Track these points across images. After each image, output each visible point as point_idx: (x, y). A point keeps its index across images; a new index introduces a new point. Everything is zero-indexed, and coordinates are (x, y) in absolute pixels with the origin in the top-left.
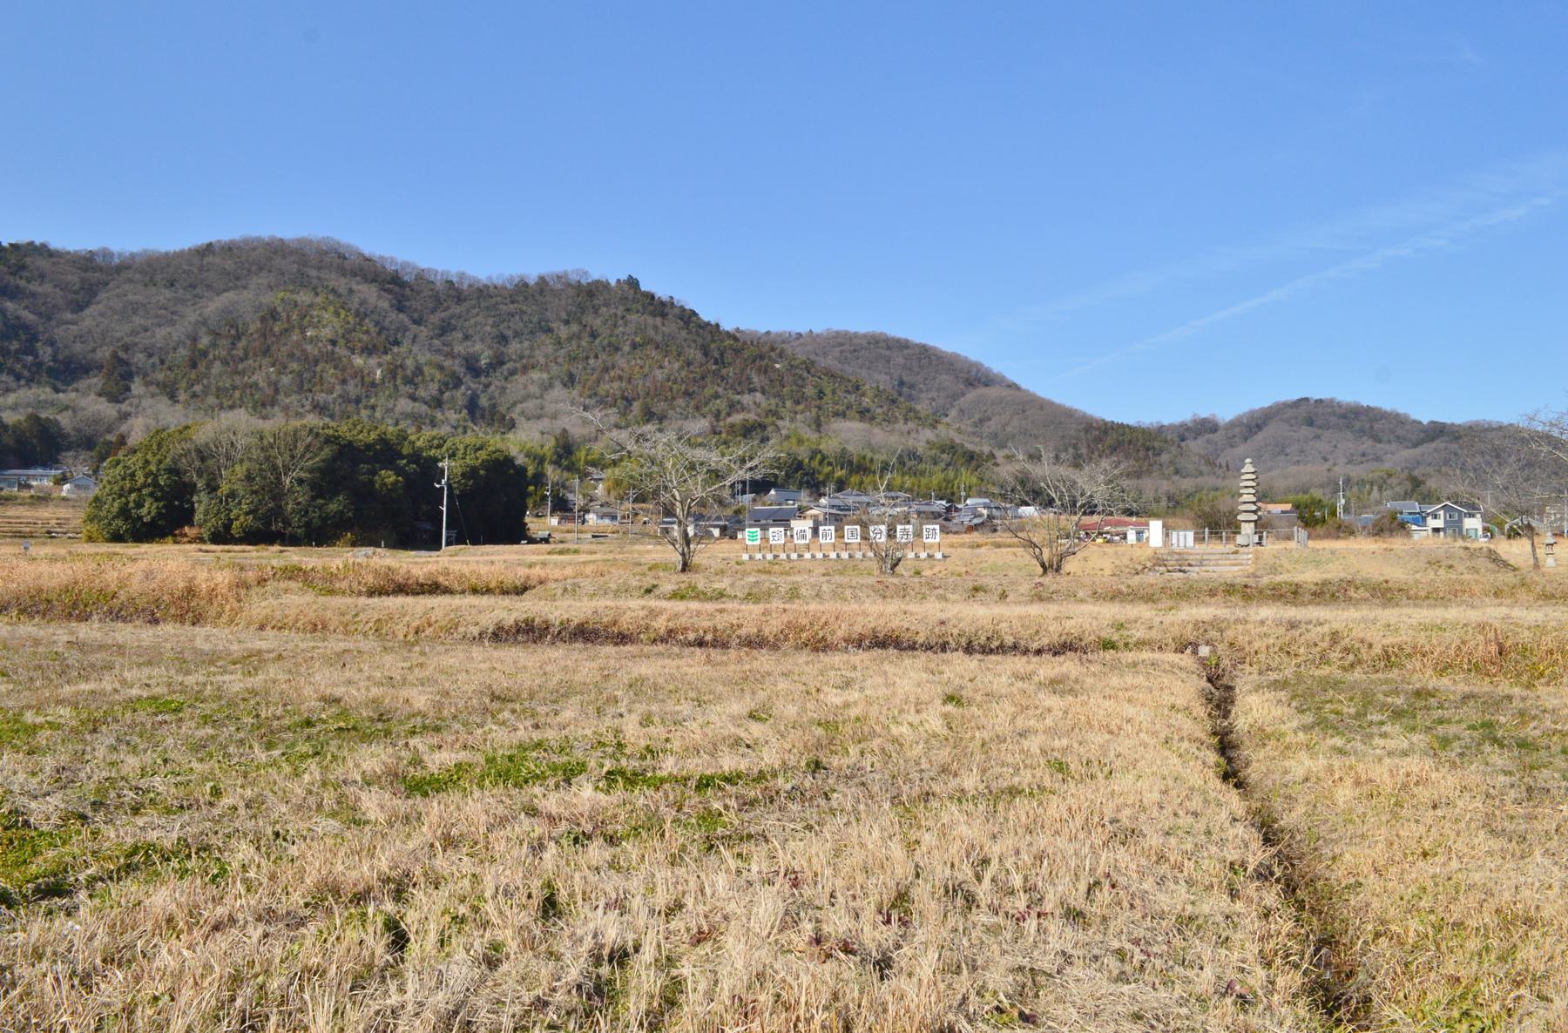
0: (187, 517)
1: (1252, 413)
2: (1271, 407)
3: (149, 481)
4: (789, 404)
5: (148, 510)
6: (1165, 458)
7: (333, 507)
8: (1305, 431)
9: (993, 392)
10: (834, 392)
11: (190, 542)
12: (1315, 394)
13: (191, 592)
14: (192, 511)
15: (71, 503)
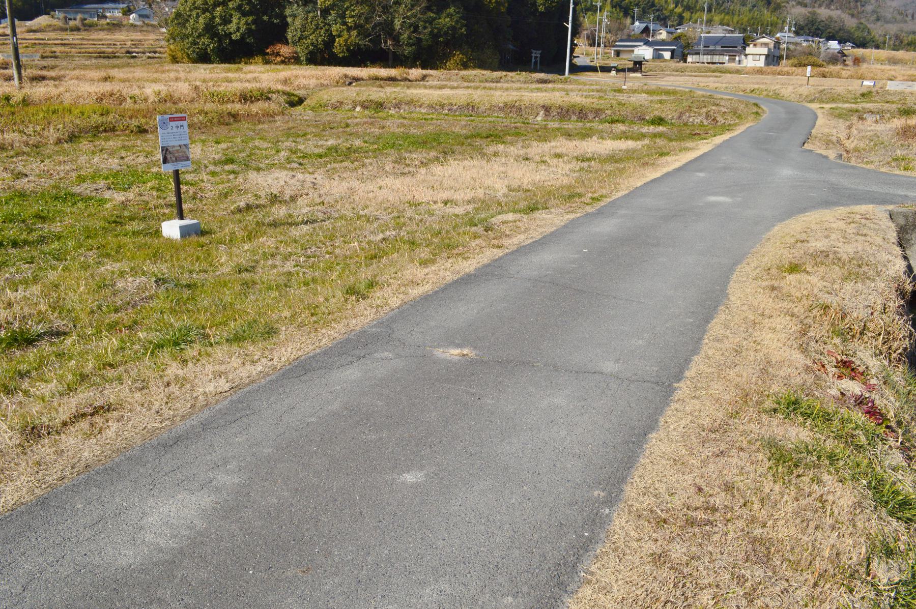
0: (278, 34)
5: (237, 26)
7: (445, 21)
11: (283, 62)
14: (285, 25)
15: (138, 29)
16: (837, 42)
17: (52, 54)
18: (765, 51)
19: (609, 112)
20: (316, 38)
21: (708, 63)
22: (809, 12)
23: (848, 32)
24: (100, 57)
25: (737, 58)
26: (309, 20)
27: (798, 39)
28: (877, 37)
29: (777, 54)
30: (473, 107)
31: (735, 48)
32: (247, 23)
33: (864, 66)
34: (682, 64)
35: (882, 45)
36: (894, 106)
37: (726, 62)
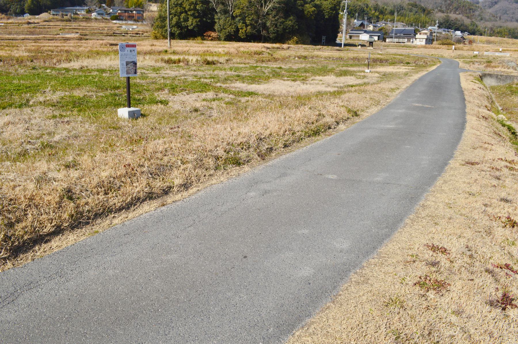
0: (211, 27)
3: (192, 7)
5: (191, 23)
6: (477, 13)
7: (289, 23)
11: (212, 40)
13: (213, 61)
16: (460, 32)
18: (425, 37)
19: (390, 61)
20: (231, 29)
21: (397, 42)
23: (466, 26)
24: (108, 35)
25: (411, 40)
26: (227, 21)
27: (440, 30)
28: (481, 29)
29: (431, 38)
30: (341, 59)
31: (411, 35)
32: (196, 22)
33: (474, 44)
34: (383, 43)
35: (483, 34)
36: (485, 60)
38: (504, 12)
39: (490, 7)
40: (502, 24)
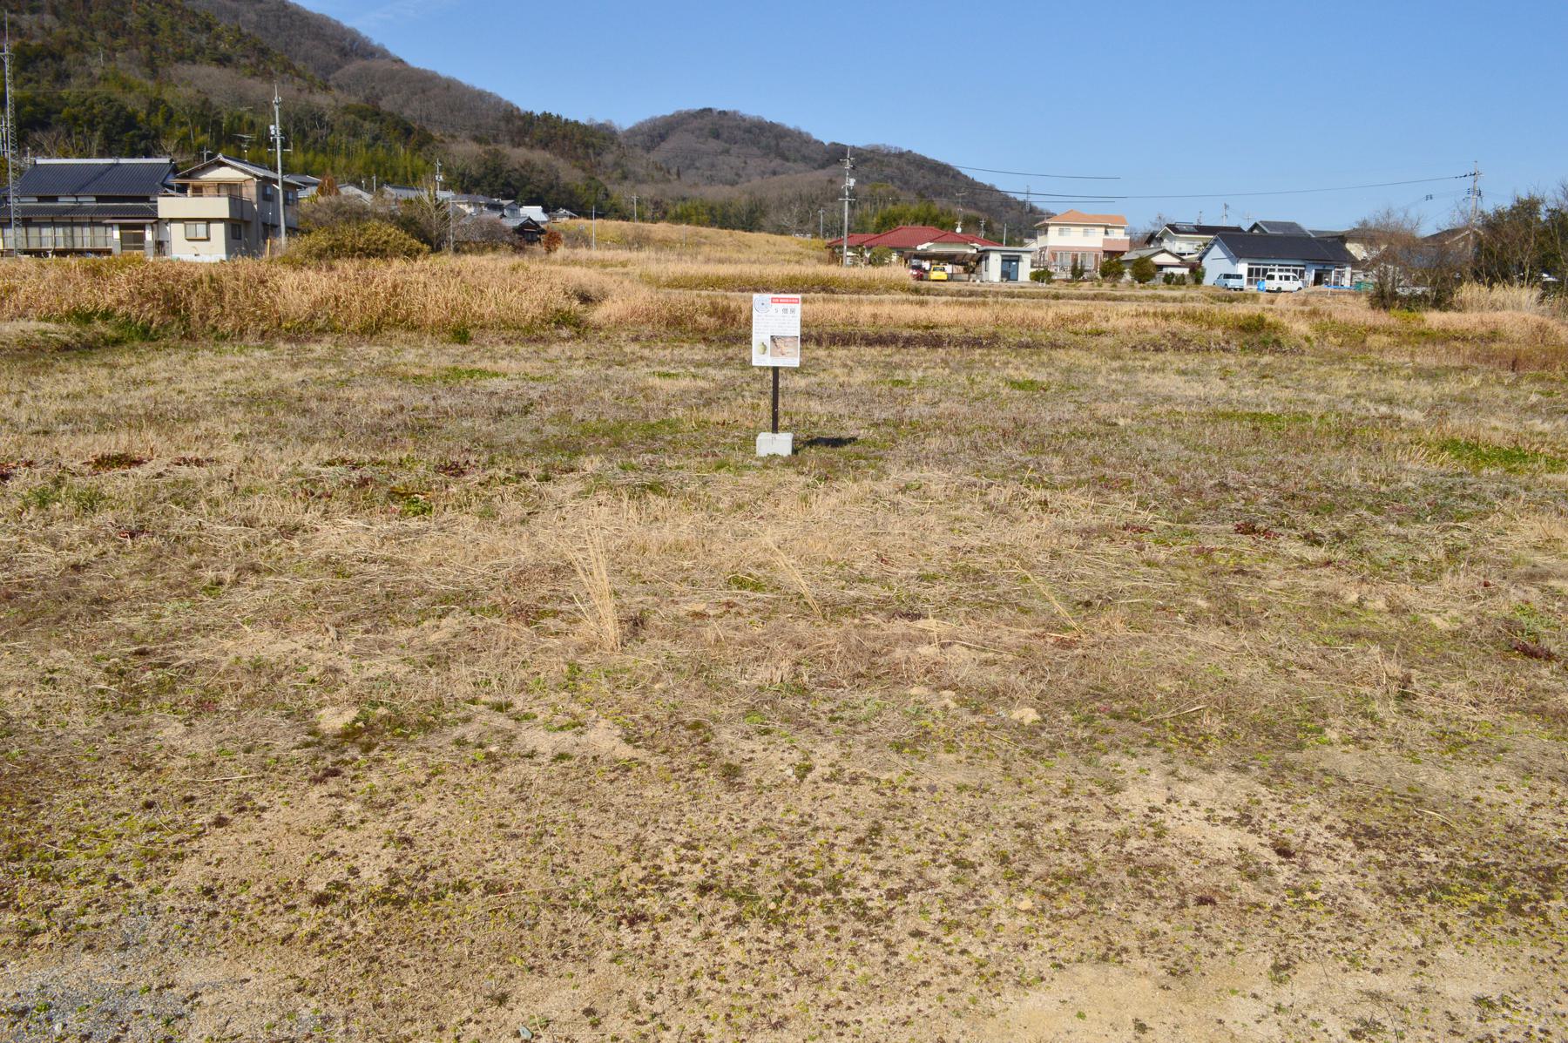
1: (654, 121)
2: (673, 116)
4: (101, 35)
6: (608, 158)
8: (714, 144)
9: (375, 64)
10: (173, 28)
12: (719, 105)
17: (926, 298)
22: (485, 152)
25: (149, 235)
37: (117, 250)
38: (687, 162)
39: (648, 150)
40: (687, 192)
